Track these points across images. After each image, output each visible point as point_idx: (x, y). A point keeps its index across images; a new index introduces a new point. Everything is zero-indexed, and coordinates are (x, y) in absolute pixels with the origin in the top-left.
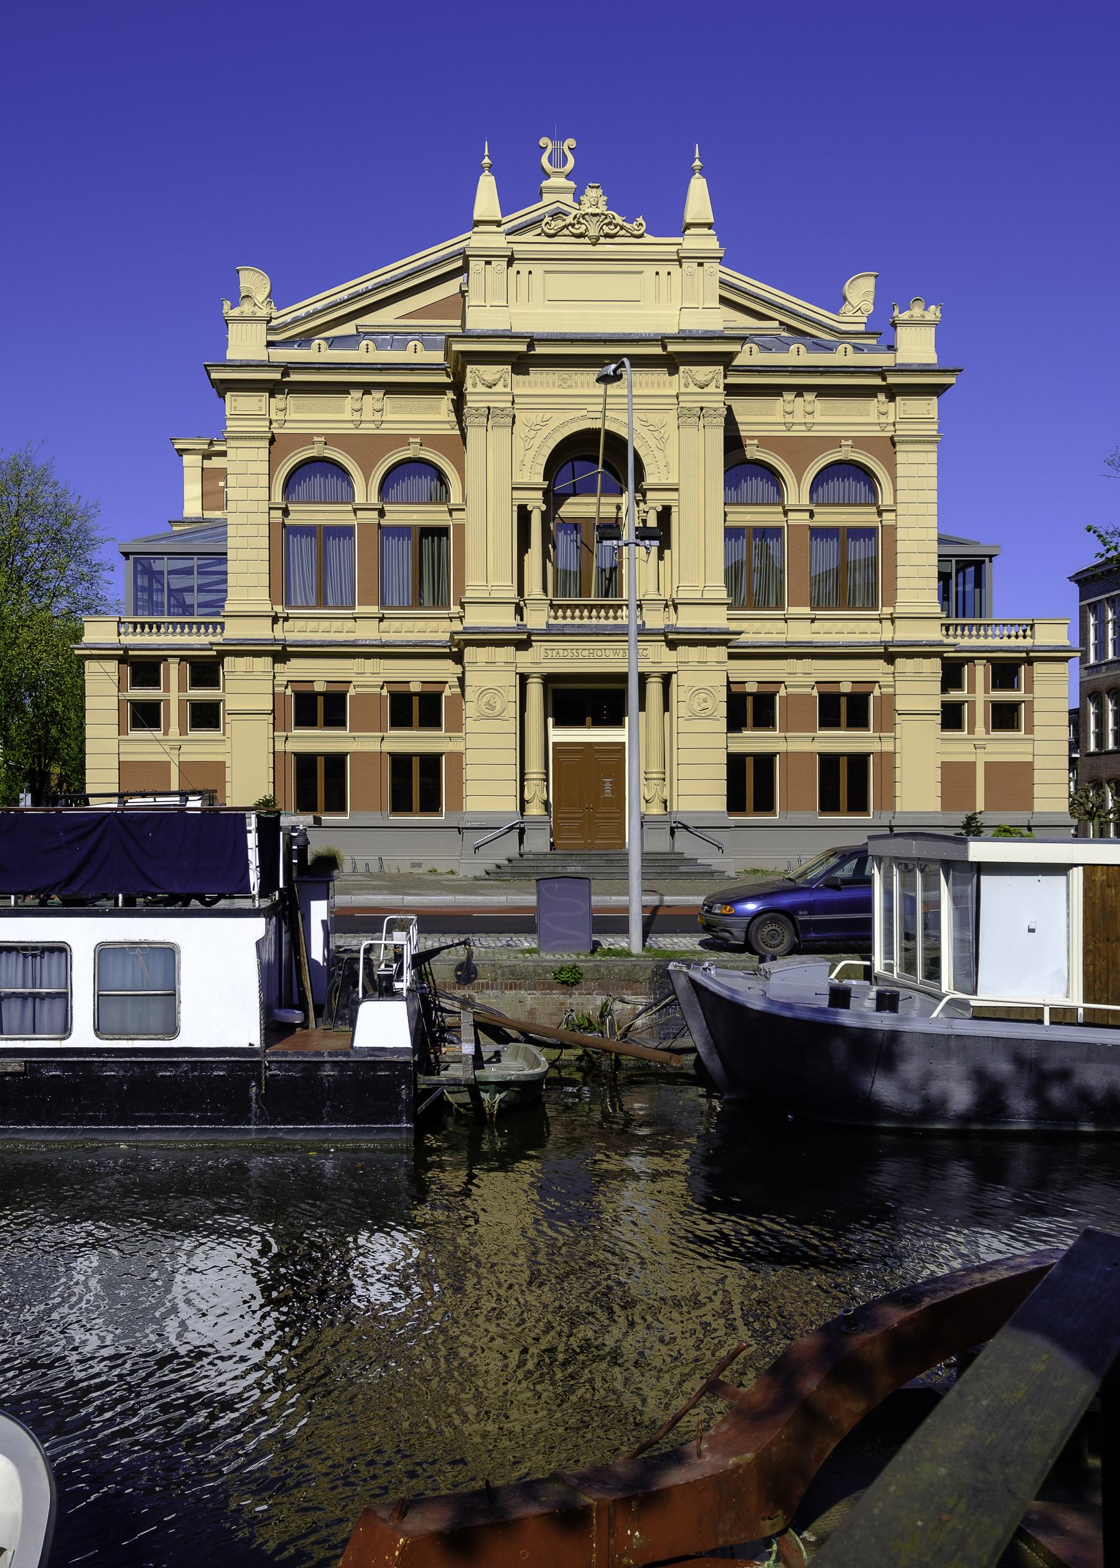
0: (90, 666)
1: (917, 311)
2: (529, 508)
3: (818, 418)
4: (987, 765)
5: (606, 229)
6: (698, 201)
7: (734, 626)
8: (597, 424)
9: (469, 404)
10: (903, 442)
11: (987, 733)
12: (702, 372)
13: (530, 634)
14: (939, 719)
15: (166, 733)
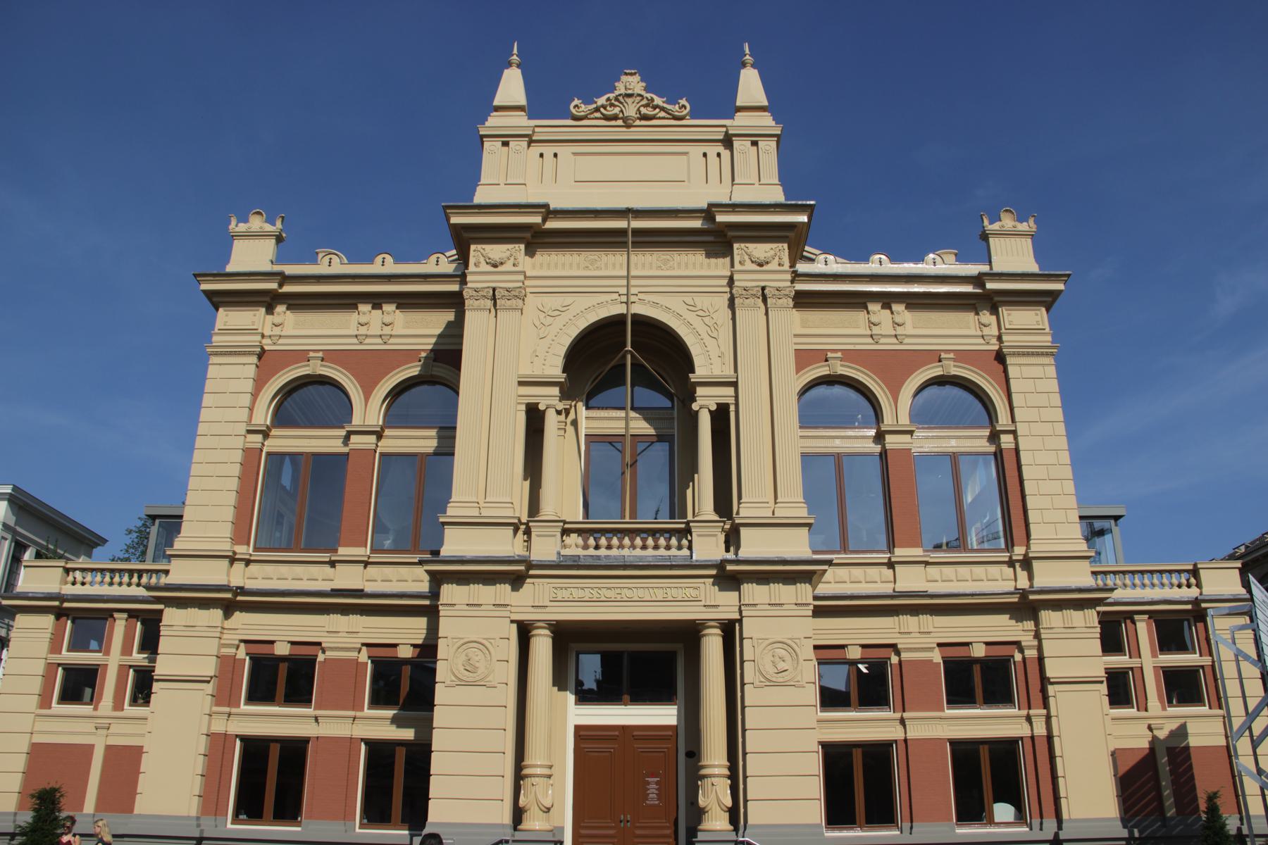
1: (1007, 222)
2: (541, 407)
3: (908, 329)
4: (109, 748)
5: (643, 110)
6: (751, 87)
8: (621, 309)
9: (469, 285)
10: (1014, 354)
11: (1164, 709)
12: (761, 250)
13: (530, 565)
14: (1103, 688)
15: (96, 709)
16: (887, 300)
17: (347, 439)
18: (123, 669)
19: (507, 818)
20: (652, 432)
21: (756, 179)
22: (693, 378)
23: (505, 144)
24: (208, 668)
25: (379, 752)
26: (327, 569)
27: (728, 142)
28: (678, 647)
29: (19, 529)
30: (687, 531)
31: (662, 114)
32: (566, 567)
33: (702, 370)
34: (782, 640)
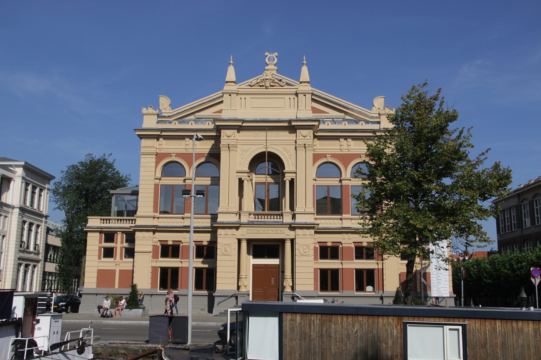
0: (89, 234)
3: (352, 147)
4: (120, 270)
5: (272, 84)
6: (305, 70)
7: (318, 222)
8: (264, 150)
12: (305, 132)
13: (241, 224)
15: (115, 259)
16: (346, 138)
17: (185, 180)
18: (122, 248)
19: (236, 288)
20: (273, 181)
21: (304, 111)
22: (284, 171)
23: (230, 95)
24: (150, 249)
25: (199, 271)
26: (181, 219)
27: (297, 94)
28: (280, 243)
29: (27, 178)
30: (282, 215)
31: (277, 85)
32: (250, 224)
33: (287, 169)
34: (306, 243)
